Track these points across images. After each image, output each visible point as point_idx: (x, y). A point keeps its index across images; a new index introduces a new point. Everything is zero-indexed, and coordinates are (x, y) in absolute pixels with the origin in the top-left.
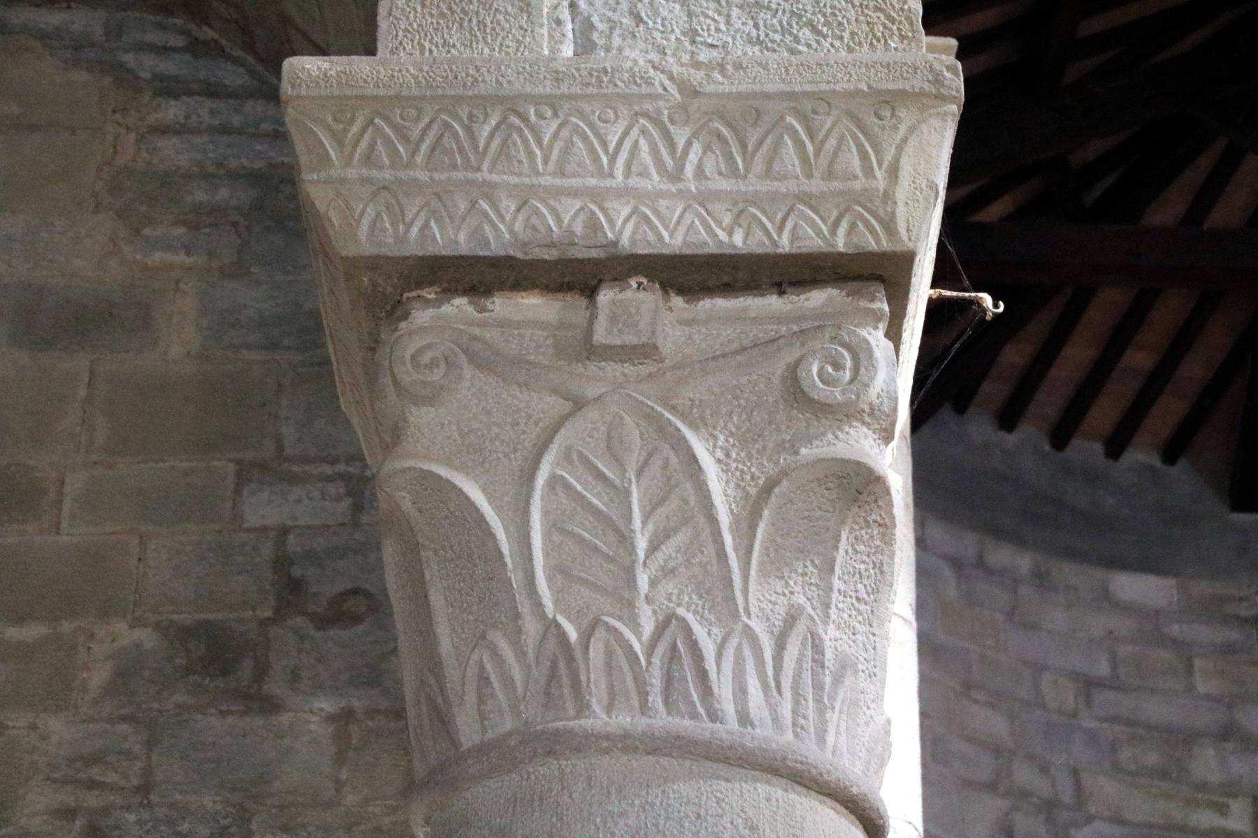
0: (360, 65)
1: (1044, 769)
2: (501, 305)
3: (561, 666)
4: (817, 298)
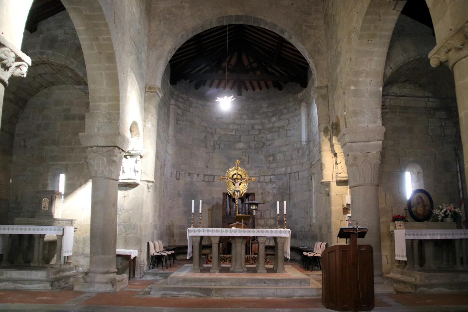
0: (83, 133)
1: (211, 129)
2: (93, 148)
3: (96, 172)
4: (112, 148)
